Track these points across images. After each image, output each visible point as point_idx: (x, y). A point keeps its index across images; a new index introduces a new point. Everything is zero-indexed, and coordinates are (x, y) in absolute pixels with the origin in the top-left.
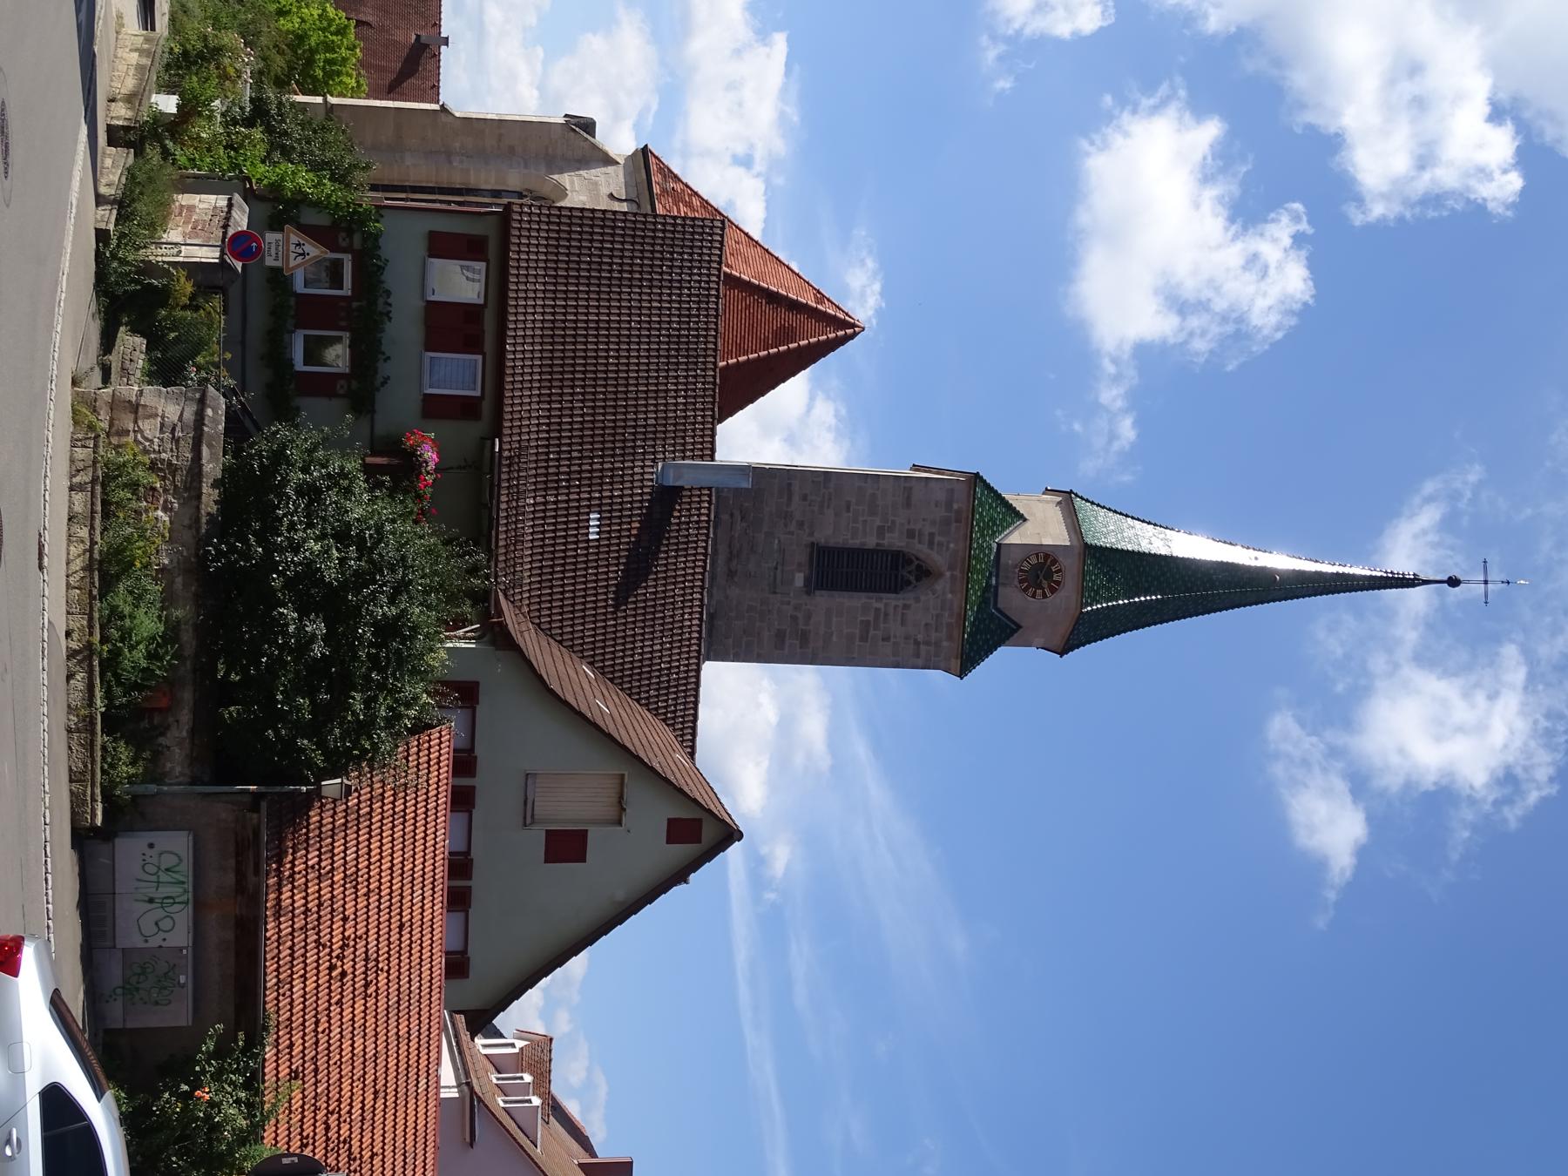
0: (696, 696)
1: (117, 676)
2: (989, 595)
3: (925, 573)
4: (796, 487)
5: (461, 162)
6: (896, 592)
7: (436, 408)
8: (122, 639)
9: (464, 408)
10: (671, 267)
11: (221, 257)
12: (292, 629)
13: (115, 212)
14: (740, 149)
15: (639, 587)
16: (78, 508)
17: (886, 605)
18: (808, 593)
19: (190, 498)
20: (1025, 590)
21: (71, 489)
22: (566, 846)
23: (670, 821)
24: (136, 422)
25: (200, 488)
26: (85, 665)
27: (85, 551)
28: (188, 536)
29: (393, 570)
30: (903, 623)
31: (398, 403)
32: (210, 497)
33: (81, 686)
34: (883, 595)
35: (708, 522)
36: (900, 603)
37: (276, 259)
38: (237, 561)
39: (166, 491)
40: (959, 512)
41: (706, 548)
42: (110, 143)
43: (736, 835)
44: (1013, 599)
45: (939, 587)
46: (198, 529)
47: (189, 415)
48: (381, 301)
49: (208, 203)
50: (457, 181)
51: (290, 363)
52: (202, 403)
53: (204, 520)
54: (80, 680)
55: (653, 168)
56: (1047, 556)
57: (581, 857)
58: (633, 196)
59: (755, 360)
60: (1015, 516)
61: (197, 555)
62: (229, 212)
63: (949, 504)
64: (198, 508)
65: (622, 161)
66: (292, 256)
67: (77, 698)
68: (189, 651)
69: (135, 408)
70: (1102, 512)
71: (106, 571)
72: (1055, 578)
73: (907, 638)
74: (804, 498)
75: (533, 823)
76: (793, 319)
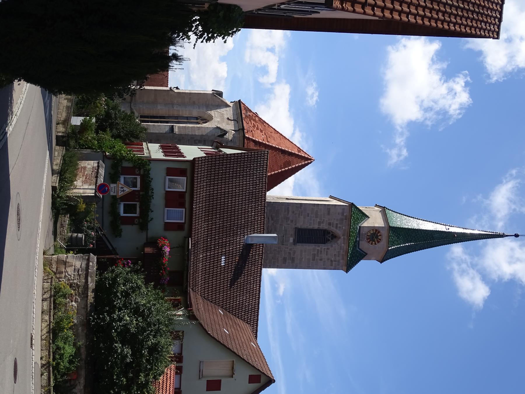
0: (258, 313)
1: (58, 372)
2: (357, 244)
4: (290, 209)
5: (177, 107)
6: (324, 243)
7: (168, 227)
8: (60, 359)
9: (179, 227)
10: (250, 169)
11: (95, 193)
13: (58, 177)
14: (270, 46)
15: (238, 279)
19: (84, 297)
20: (369, 242)
21: (43, 300)
23: (250, 376)
24: (65, 268)
26: (47, 370)
27: (47, 325)
28: (83, 312)
31: (156, 227)
32: (91, 295)
33: (46, 378)
34: (320, 245)
35: (262, 253)
36: (326, 247)
38: (100, 323)
40: (346, 216)
41: (261, 262)
42: (57, 144)
44: (364, 245)
45: (339, 242)
46: (87, 309)
47: (84, 265)
48: (150, 192)
50: (176, 114)
51: (119, 214)
52: (88, 260)
53: (89, 306)
54: (45, 376)
55: (243, 108)
56: (376, 230)
57: (219, 389)
58: (236, 118)
59: (277, 173)
61: (86, 319)
63: (343, 214)
64: (87, 301)
65: (231, 105)
66: (120, 191)
67: (44, 383)
68: (83, 356)
69: (65, 263)
70: (395, 214)
71: (54, 332)
73: (328, 259)
75: (202, 377)
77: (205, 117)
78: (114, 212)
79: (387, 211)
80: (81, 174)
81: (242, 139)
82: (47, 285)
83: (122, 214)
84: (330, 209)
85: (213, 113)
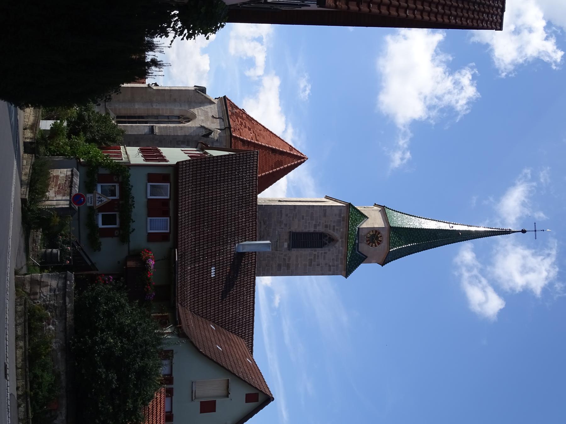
2: (356, 247)
3: (332, 240)
4: (284, 212)
6: (321, 247)
7: (152, 238)
9: (163, 237)
12: (104, 376)
13: (28, 189)
15: (230, 291)
16: (19, 333)
17: (318, 253)
18: (289, 250)
20: (369, 244)
21: (16, 325)
22: (208, 407)
24: (40, 289)
25: (66, 315)
29: (141, 347)
30: (324, 259)
36: (323, 252)
37: (91, 203)
39: (53, 317)
40: (343, 218)
42: (25, 152)
43: (272, 399)
44: (364, 248)
45: (337, 245)
48: (130, 200)
49: (63, 173)
52: (66, 279)
54: (22, 409)
55: (228, 105)
56: (376, 231)
57: (214, 410)
58: (221, 116)
59: (268, 174)
60: (364, 217)
62: (72, 178)
63: (340, 215)
64: (65, 323)
66: (97, 202)
67: (22, 416)
69: (40, 283)
70: (396, 213)
72: (379, 239)
73: (326, 264)
74: (287, 215)
76: (278, 157)
77: (188, 115)
78: (91, 224)
79: (387, 210)
80: (53, 184)
81: (228, 138)
82: (20, 308)
83: (101, 226)
84: (326, 210)
85: (196, 111)
